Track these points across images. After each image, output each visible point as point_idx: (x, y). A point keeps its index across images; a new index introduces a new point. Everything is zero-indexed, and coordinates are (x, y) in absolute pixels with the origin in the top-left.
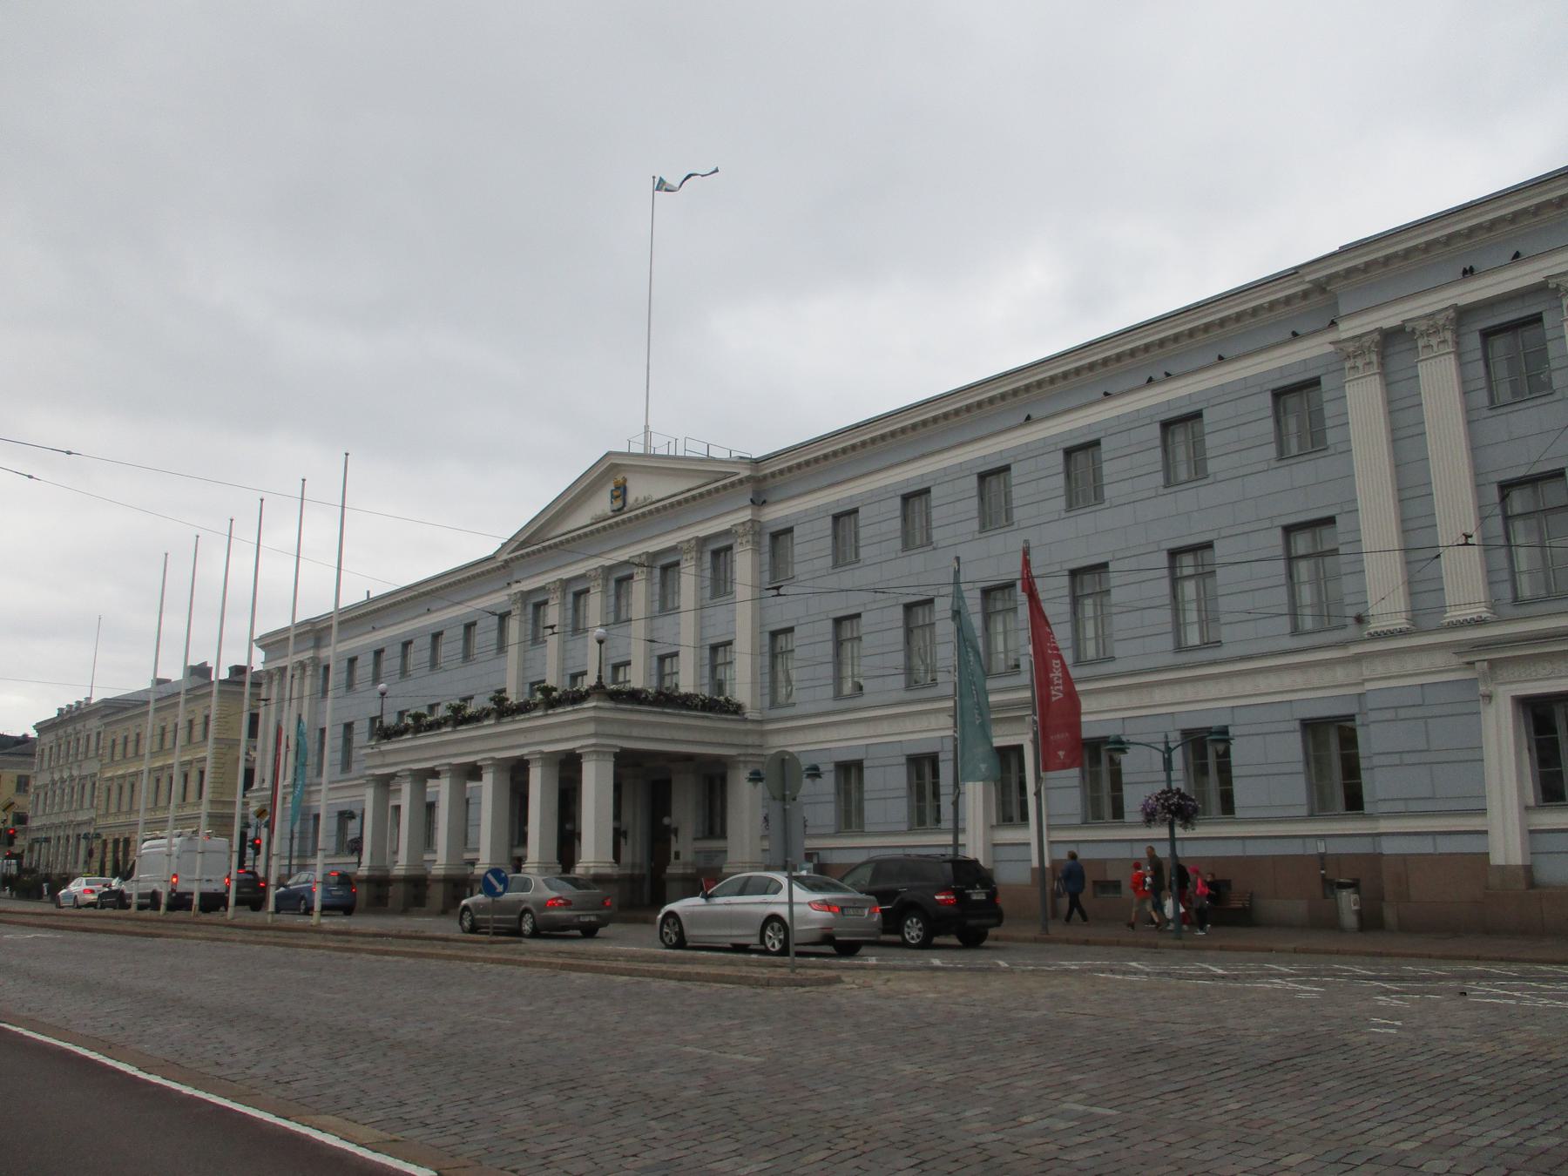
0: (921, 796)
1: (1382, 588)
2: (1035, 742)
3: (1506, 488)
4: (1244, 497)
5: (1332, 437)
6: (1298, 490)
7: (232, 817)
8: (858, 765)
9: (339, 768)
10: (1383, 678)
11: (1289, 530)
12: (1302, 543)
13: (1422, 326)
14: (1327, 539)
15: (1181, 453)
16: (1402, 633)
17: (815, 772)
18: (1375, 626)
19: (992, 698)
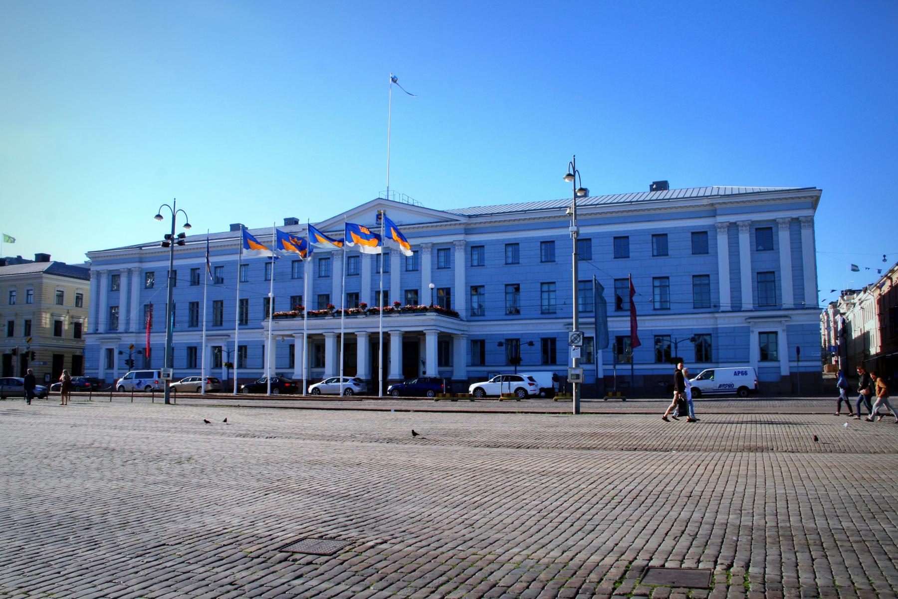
0: (191, 356)
1: (725, 298)
2: (882, 330)
3: (406, 291)
4: (681, 264)
5: (774, 246)
6: (699, 265)
7: (238, 368)
8: (245, 347)
9: (211, 324)
10: (726, 321)
11: (542, 284)
12: (545, 288)
13: (424, 246)
14: (552, 287)
15: (475, 257)
16: (751, 311)
17: (531, 344)
18: (722, 309)
19: (593, 320)
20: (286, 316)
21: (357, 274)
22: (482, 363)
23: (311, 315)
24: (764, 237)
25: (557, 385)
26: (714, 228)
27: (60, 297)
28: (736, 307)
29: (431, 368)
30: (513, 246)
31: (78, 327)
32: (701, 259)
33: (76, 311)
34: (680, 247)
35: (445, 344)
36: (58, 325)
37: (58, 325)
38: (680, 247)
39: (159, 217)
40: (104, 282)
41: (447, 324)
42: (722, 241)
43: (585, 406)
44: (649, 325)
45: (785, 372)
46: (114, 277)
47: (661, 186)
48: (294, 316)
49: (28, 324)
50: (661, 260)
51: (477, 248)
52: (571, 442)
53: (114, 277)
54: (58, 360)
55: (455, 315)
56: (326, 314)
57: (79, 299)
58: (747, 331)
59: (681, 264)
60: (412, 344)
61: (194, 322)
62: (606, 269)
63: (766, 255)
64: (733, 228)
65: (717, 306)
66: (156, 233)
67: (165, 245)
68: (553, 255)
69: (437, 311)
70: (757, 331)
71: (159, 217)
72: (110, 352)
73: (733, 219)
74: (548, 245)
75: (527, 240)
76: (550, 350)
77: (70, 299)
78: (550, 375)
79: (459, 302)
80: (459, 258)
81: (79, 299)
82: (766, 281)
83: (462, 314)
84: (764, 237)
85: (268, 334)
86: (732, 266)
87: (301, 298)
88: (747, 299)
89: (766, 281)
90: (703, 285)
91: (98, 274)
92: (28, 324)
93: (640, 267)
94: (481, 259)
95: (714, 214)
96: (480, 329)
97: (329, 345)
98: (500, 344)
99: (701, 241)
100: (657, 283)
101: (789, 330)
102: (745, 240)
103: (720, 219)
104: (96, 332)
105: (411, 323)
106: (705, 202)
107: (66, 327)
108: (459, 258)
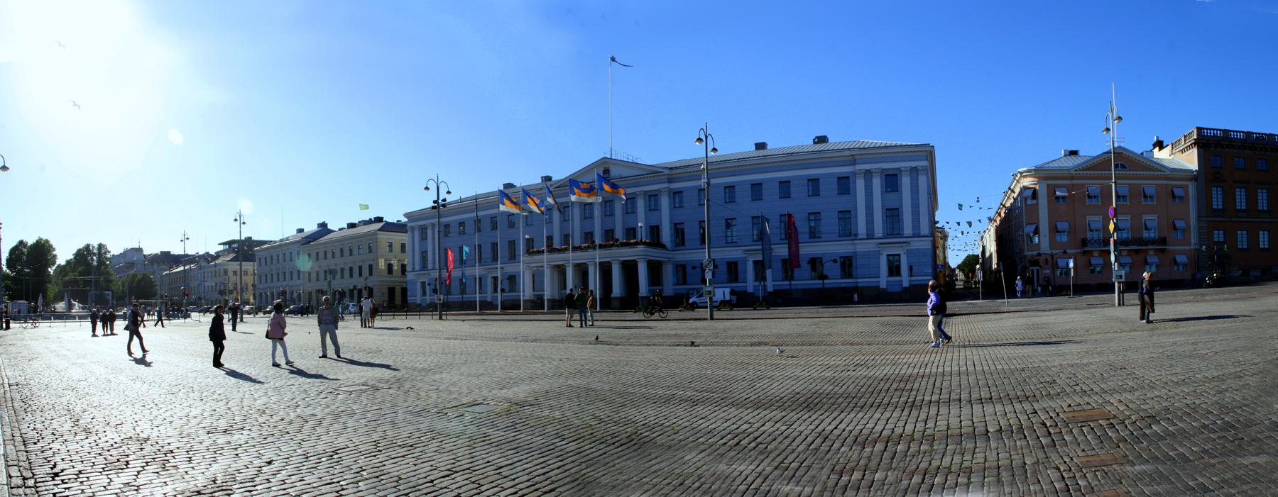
1: (862, 229)
4: (829, 203)
6: (843, 203)
10: (863, 247)
17: (694, 268)
20: (559, 251)
21: (612, 215)
22: (685, 282)
23: (601, 246)
24: (891, 181)
25: (734, 298)
26: (854, 174)
27: (391, 245)
28: (870, 236)
29: (643, 289)
30: (730, 188)
31: (404, 267)
32: (844, 198)
33: (402, 256)
34: (829, 188)
35: (655, 269)
36: (390, 267)
37: (390, 267)
38: (829, 188)
39: (427, 188)
40: (417, 234)
41: (655, 254)
42: (860, 184)
43: (717, 314)
44: (808, 249)
45: (906, 284)
46: (423, 230)
47: (822, 140)
48: (587, 248)
49: (371, 267)
50: (815, 199)
51: (677, 193)
52: (748, 340)
53: (423, 230)
54: (391, 291)
55: (663, 246)
56: (612, 246)
57: (403, 246)
58: (878, 254)
59: (829, 203)
60: (630, 269)
61: (513, 257)
62: (772, 206)
63: (892, 195)
64: (868, 174)
65: (856, 235)
66: (426, 202)
67: (433, 208)
68: (734, 197)
69: (645, 243)
70: (885, 254)
71: (427, 188)
72: (423, 283)
73: (868, 167)
74: (814, 182)
75: (797, 178)
76: (733, 270)
77: (397, 248)
78: (727, 291)
79: (666, 236)
80: (665, 202)
81: (403, 246)
82: (893, 214)
83: (669, 245)
84: (891, 181)
85: (523, 267)
86: (867, 203)
87: (592, 234)
88: (879, 230)
89: (893, 214)
90: (846, 216)
91: (413, 228)
92: (371, 267)
93: (799, 206)
94: (681, 202)
95: (854, 163)
96: (683, 256)
97: (591, 270)
98: (835, 261)
99: (844, 184)
100: (812, 217)
101: (909, 253)
102: (877, 182)
103: (858, 167)
104: (413, 270)
105: (628, 254)
106: (847, 153)
107: (395, 268)
108: (665, 202)
